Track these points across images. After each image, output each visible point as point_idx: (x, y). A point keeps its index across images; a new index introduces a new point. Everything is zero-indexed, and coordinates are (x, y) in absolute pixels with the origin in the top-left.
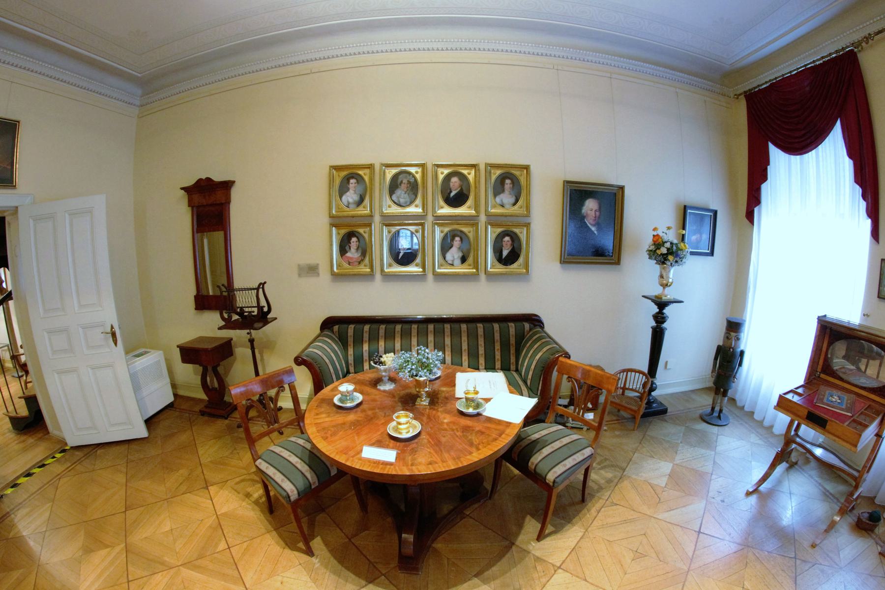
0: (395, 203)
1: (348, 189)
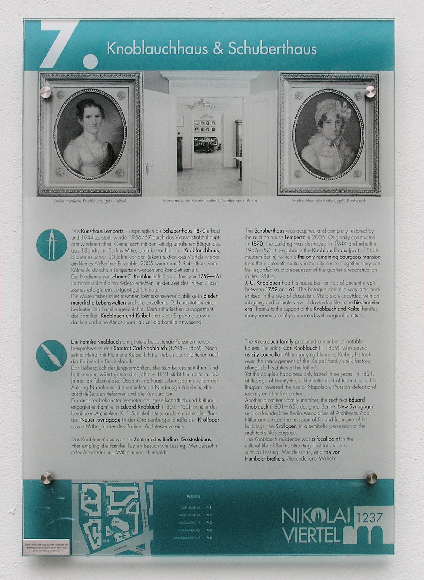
0: (309, 167)
1: (79, 131)
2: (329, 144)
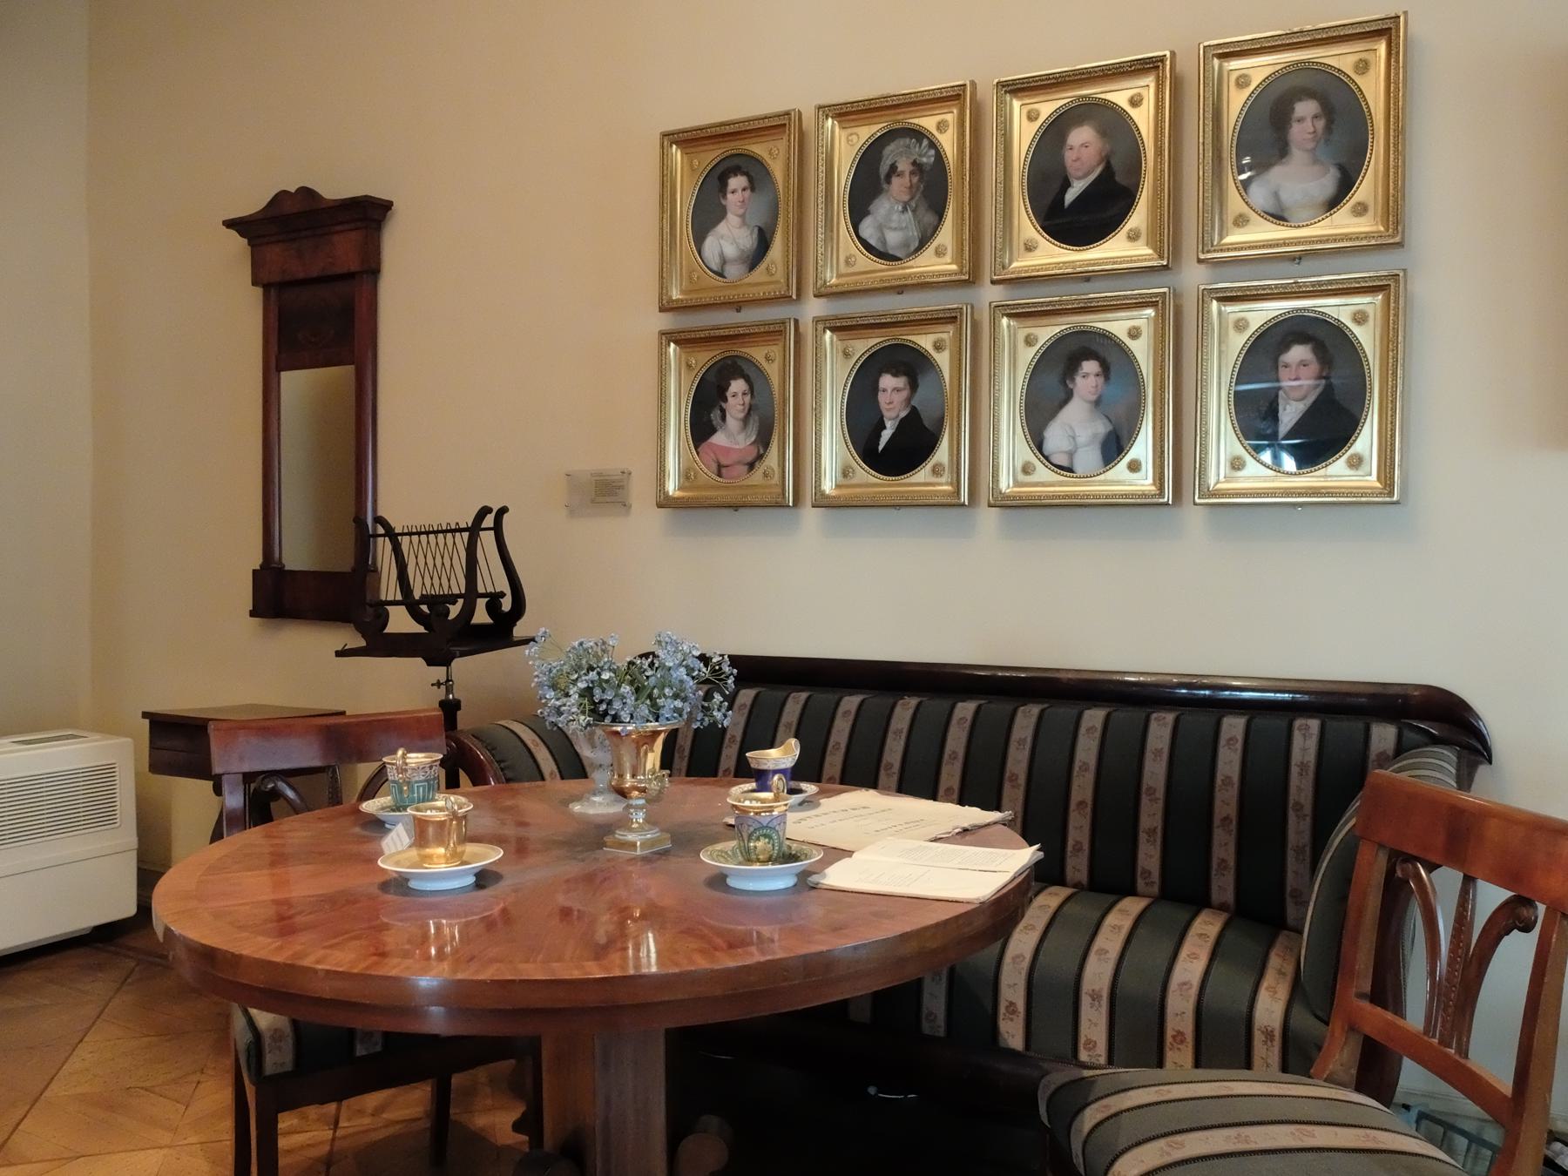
1: (721, 214)
2: (900, 208)
